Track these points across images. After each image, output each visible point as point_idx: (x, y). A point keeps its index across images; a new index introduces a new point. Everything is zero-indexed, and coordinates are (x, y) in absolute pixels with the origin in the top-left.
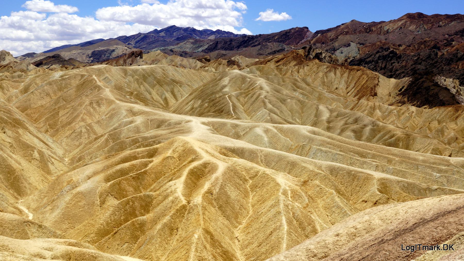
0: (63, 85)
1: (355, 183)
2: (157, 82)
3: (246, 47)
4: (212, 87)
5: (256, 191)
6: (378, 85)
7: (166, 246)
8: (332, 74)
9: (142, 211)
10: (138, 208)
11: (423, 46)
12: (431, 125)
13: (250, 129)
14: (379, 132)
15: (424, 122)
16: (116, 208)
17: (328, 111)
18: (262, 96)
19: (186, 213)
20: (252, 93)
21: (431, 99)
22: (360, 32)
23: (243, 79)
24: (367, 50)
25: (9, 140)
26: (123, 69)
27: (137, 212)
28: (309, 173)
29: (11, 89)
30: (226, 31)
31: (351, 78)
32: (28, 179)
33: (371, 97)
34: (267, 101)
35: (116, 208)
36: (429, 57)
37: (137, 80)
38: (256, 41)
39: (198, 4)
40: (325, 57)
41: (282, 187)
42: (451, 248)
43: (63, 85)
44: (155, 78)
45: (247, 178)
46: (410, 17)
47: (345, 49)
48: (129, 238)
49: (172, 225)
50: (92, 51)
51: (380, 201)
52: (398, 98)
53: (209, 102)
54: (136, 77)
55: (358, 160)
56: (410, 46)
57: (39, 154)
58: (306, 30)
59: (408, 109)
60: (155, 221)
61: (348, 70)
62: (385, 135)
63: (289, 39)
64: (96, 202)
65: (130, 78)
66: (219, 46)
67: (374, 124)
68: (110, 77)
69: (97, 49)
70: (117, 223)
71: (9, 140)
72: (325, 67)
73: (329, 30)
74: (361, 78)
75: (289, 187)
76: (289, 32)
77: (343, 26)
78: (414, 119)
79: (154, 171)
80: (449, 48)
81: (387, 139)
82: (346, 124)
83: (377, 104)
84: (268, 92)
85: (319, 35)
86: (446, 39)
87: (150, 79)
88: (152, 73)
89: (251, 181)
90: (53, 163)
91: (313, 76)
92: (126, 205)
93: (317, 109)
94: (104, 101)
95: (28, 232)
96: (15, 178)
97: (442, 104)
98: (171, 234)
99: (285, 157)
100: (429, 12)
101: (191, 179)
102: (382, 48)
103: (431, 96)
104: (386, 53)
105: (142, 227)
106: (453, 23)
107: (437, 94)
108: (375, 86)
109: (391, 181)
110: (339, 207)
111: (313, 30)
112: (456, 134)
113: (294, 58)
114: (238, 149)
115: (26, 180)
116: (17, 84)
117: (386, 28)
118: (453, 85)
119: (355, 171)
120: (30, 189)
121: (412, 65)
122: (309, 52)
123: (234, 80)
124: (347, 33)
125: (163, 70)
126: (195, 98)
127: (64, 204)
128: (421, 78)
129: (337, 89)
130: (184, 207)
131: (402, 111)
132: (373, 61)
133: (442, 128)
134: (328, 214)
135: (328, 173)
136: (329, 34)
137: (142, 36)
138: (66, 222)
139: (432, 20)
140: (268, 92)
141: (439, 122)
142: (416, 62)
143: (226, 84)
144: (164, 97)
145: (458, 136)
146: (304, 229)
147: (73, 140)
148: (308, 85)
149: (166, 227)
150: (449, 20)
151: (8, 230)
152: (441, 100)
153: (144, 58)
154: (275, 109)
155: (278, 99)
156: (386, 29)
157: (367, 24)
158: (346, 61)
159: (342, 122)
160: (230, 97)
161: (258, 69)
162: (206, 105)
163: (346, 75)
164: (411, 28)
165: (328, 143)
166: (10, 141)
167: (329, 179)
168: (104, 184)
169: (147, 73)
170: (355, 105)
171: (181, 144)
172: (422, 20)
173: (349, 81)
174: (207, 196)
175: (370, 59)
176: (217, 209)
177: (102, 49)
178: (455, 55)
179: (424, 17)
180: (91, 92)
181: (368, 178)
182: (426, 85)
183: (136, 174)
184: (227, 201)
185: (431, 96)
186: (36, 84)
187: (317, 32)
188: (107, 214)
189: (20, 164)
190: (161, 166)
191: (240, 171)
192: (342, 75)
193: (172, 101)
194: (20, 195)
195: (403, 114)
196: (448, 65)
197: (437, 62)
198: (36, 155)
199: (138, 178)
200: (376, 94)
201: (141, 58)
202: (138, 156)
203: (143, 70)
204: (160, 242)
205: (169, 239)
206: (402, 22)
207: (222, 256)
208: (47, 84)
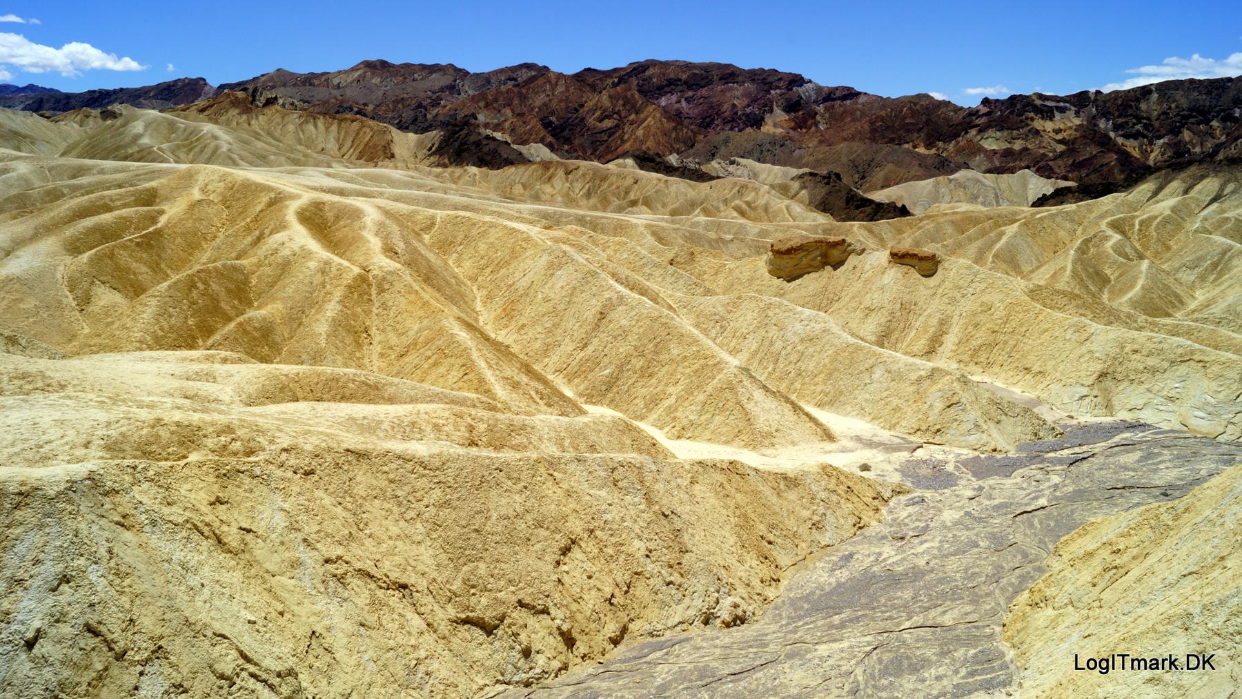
4: (111, 137)
5: (456, 252)
8: (311, 127)
9: (236, 302)
11: (400, 106)
16: (167, 299)
19: (374, 291)
30: (48, 87)
35: (167, 299)
42: (1207, 665)
46: (369, 65)
49: (352, 322)
58: (202, 82)
59: (465, 171)
61: (336, 121)
63: (175, 96)
64: (65, 301)
70: (181, 336)
74: (362, 133)
77: (263, 79)
79: (180, 231)
84: (230, 144)
92: (190, 290)
98: (359, 345)
100: (396, 59)
103: (487, 154)
106: (434, 75)
111: (214, 82)
117: (336, 81)
149: (340, 328)
150: (427, 71)
156: (335, 83)
163: (334, 128)
168: (68, 260)
173: (342, 137)
183: (141, 237)
187: (222, 87)
188: (144, 316)
190: (190, 221)
192: (327, 129)
199: (150, 246)
200: (393, 156)
202: (112, 204)
205: (358, 355)
206: (359, 72)
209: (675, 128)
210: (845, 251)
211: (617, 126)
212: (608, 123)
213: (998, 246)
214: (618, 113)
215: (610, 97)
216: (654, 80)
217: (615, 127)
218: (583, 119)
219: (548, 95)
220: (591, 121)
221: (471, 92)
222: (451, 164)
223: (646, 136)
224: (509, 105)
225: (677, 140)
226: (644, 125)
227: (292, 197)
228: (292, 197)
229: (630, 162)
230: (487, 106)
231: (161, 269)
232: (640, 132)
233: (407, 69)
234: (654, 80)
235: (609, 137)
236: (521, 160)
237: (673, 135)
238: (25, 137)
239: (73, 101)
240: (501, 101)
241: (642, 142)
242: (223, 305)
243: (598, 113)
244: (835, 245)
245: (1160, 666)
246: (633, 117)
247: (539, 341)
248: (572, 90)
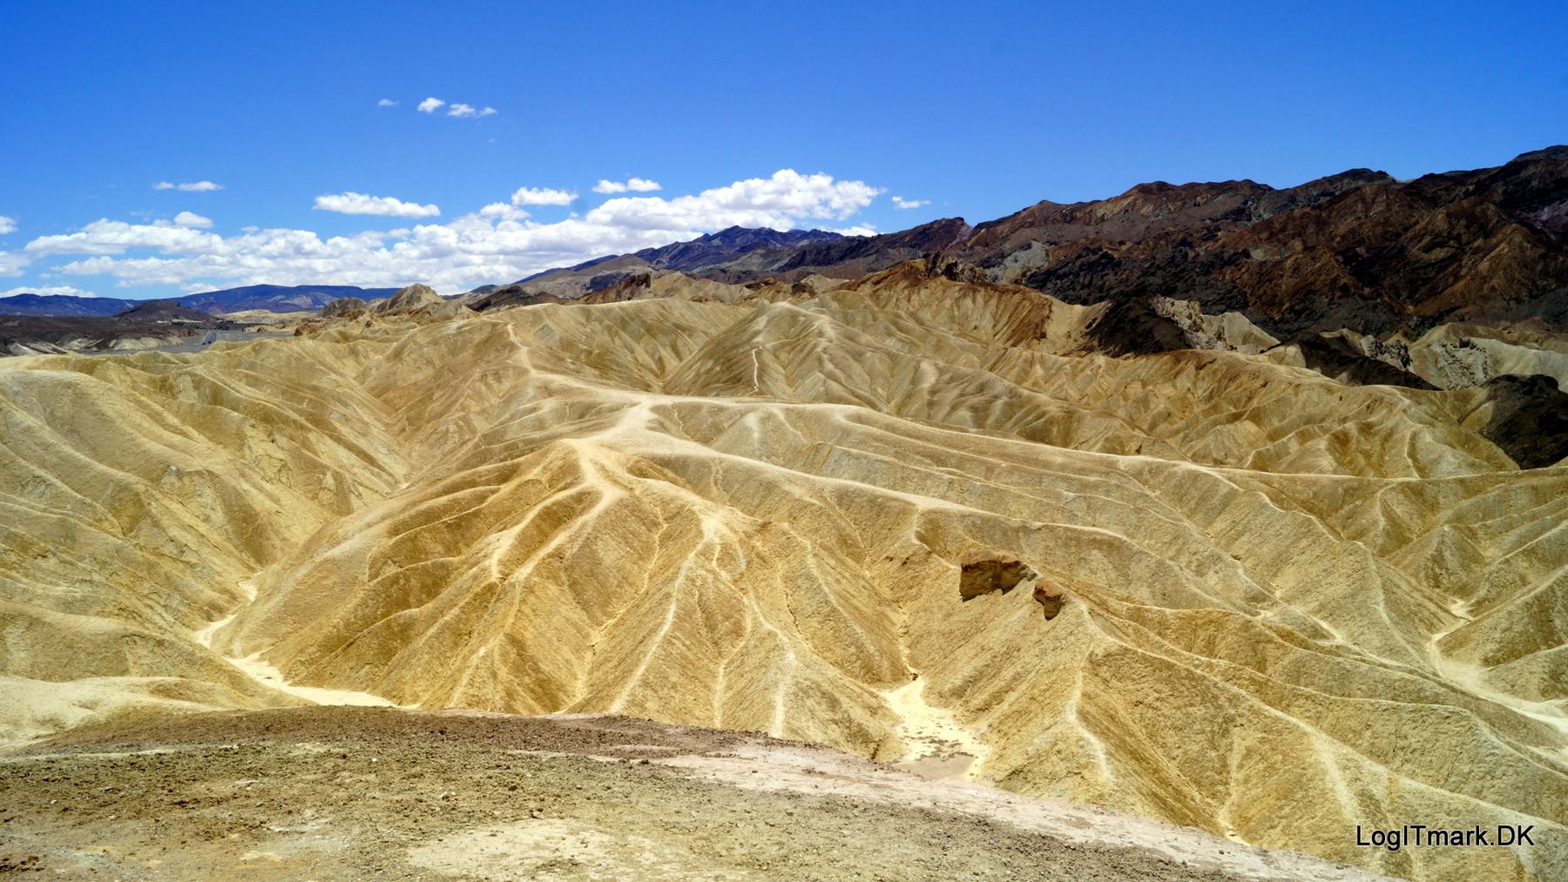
0: (459, 344)
1: (881, 521)
3: (854, 258)
6: (1048, 317)
7: (440, 670)
8: (968, 302)
10: (416, 591)
12: (1128, 390)
13: (742, 415)
14: (1022, 407)
15: (1119, 384)
17: (935, 371)
18: (819, 349)
20: (802, 342)
21: (1139, 340)
22: (1055, 221)
23: (794, 317)
24: (1061, 254)
25: (280, 455)
26: (583, 310)
27: (412, 600)
28: (791, 504)
29: (371, 355)
31: (1002, 307)
32: (283, 530)
33: (1035, 341)
34: (825, 357)
36: (1172, 261)
37: (609, 328)
40: (963, 271)
41: (706, 539)
43: (459, 344)
44: (644, 322)
45: (661, 520)
46: (1144, 190)
47: (1022, 255)
48: (375, 655)
51: (914, 558)
52: (1081, 341)
53: (723, 364)
54: (607, 322)
55: (917, 471)
56: (1139, 243)
57: (335, 479)
60: (432, 619)
62: (1028, 413)
63: (929, 240)
65: (597, 326)
66: (808, 258)
67: (1012, 393)
68: (551, 325)
71: (280, 455)
72: (957, 288)
75: (721, 537)
78: (1102, 380)
80: (1210, 244)
81: (1031, 422)
82: (962, 395)
83: (1038, 354)
84: (831, 341)
86: (1208, 229)
87: (634, 325)
88: (637, 315)
89: (666, 526)
90: (359, 496)
91: (934, 307)
93: (917, 369)
94: (511, 372)
95: (129, 656)
96: (255, 530)
97: (1158, 349)
98: (456, 644)
99: (759, 472)
100: (1177, 179)
101: (538, 526)
102: (1088, 249)
103: (1140, 335)
104: (1093, 258)
105: (405, 632)
106: (1220, 198)
107: (1151, 330)
108: (1043, 321)
109: (946, 514)
110: (809, 577)
111: (972, 222)
112: (1170, 406)
113: (905, 276)
114: (677, 459)
115: (277, 532)
116: (384, 345)
117: (1100, 213)
118: (1187, 312)
119: (884, 497)
120: (282, 550)
121: (1138, 278)
122: (934, 263)
123: (775, 321)
124: (1032, 225)
125: (663, 307)
126: (705, 356)
127: (293, 584)
128: (1126, 302)
129: (975, 328)
130: (491, 588)
131: (1081, 366)
132: (1070, 273)
133: (1146, 396)
134: (789, 592)
135: (833, 502)
136: (1000, 228)
137: (681, 247)
138: (289, 619)
139: (1184, 193)
140: (831, 341)
141: (1144, 384)
142: (1145, 273)
144: (656, 357)
145: (1173, 410)
146: (712, 628)
147: (431, 446)
148: (920, 323)
151: (82, 656)
152: (1157, 342)
153: (652, 286)
154: (837, 371)
155: (848, 352)
156: (1099, 215)
158: (1024, 275)
159: (956, 392)
160: (758, 354)
161: (835, 298)
162: (718, 369)
163: (994, 302)
164: (1144, 211)
165: (877, 439)
166: (282, 457)
167: (829, 515)
169: (628, 315)
170: (1000, 358)
171: (562, 455)
172: (1166, 195)
174: (549, 563)
175: (1066, 269)
176: (565, 587)
177: (608, 273)
178: (1219, 256)
181: (906, 510)
182: (1132, 315)
184: (592, 570)
185: (1140, 335)
186: (415, 343)
187: (980, 226)
189: (277, 501)
191: (647, 507)
193: (672, 364)
194: (260, 562)
195: (1082, 370)
196: (1205, 275)
197: (1183, 270)
198: (329, 480)
200: (1043, 336)
201: (648, 286)
202: (478, 480)
203: (622, 309)
204: (428, 663)
205: (448, 654)
206: (1129, 200)
207: (532, 691)
208: (429, 343)
209: (1543, 257)
210: (1017, 574)
211: (1454, 258)
212: (1439, 253)
213: (1548, 534)
214: (1458, 238)
215: (1448, 215)
216: (1534, 183)
217: (1449, 258)
218: (1403, 249)
219: (1359, 218)
220: (1414, 251)
221: (1266, 216)
223: (1492, 271)
224: (1300, 235)
225: (1545, 274)
226: (1493, 254)
230: (1272, 235)
232: (1484, 266)
234: (1534, 183)
235: (1438, 273)
237: (1540, 267)
239: (833, 253)
240: (1290, 231)
241: (1484, 280)
243: (1427, 239)
244: (1007, 567)
245: (1465, 841)
246: (1479, 242)
248: (1395, 208)
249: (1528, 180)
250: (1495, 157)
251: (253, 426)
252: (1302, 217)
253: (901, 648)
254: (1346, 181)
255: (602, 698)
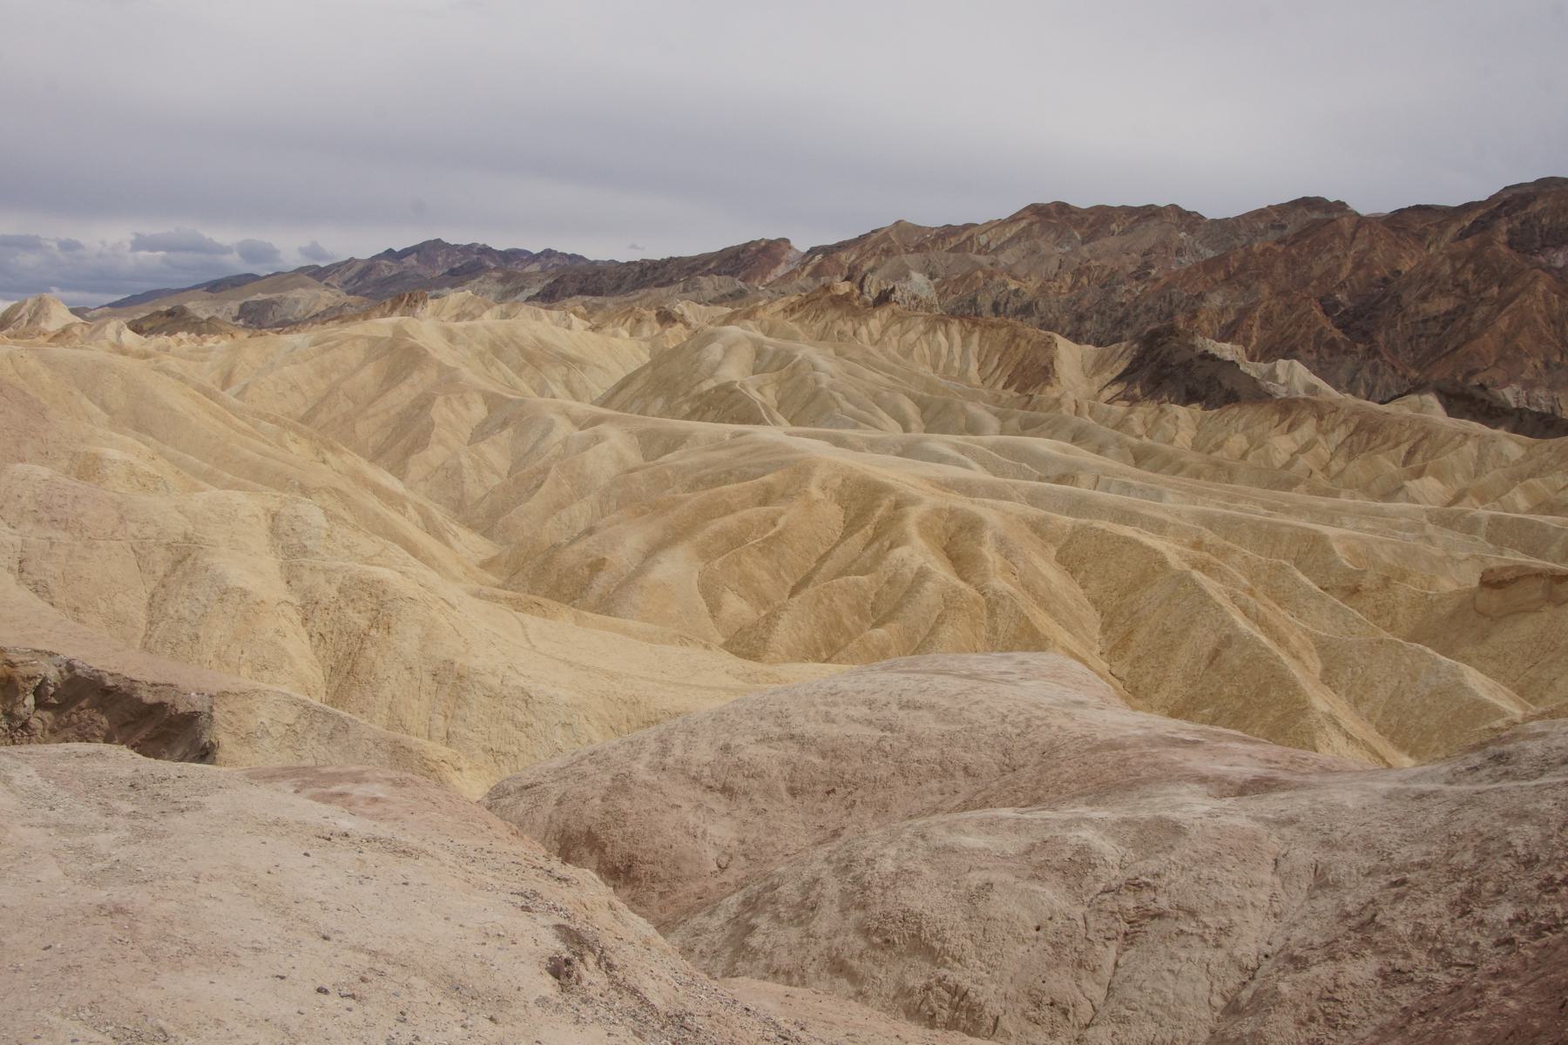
2: (528, 360)
9: (856, 618)
37: (480, 354)
38: (662, 275)
39: (133, 238)
44: (522, 349)
50: (242, 302)
69: (254, 298)
73: (842, 246)
76: (743, 251)
77: (875, 236)
85: (819, 257)
111: (802, 244)
117: (983, 240)
143: (719, 358)
157: (932, 229)
179: (1072, 212)
180: (422, 375)
187: (813, 251)
206: (1023, 224)
219: (1338, 257)
222: (1144, 396)
227: (915, 501)
228: (915, 501)
229: (1431, 399)
230: (1228, 278)
231: (780, 576)
233: (1101, 219)
236: (1258, 395)
238: (574, 361)
242: (845, 620)
247: (1150, 675)
249: (1537, 217)
250: (465, 242)
251: (295, 441)
252: (1263, 254)
253: (351, 614)
254: (1299, 211)
255: (870, 704)
